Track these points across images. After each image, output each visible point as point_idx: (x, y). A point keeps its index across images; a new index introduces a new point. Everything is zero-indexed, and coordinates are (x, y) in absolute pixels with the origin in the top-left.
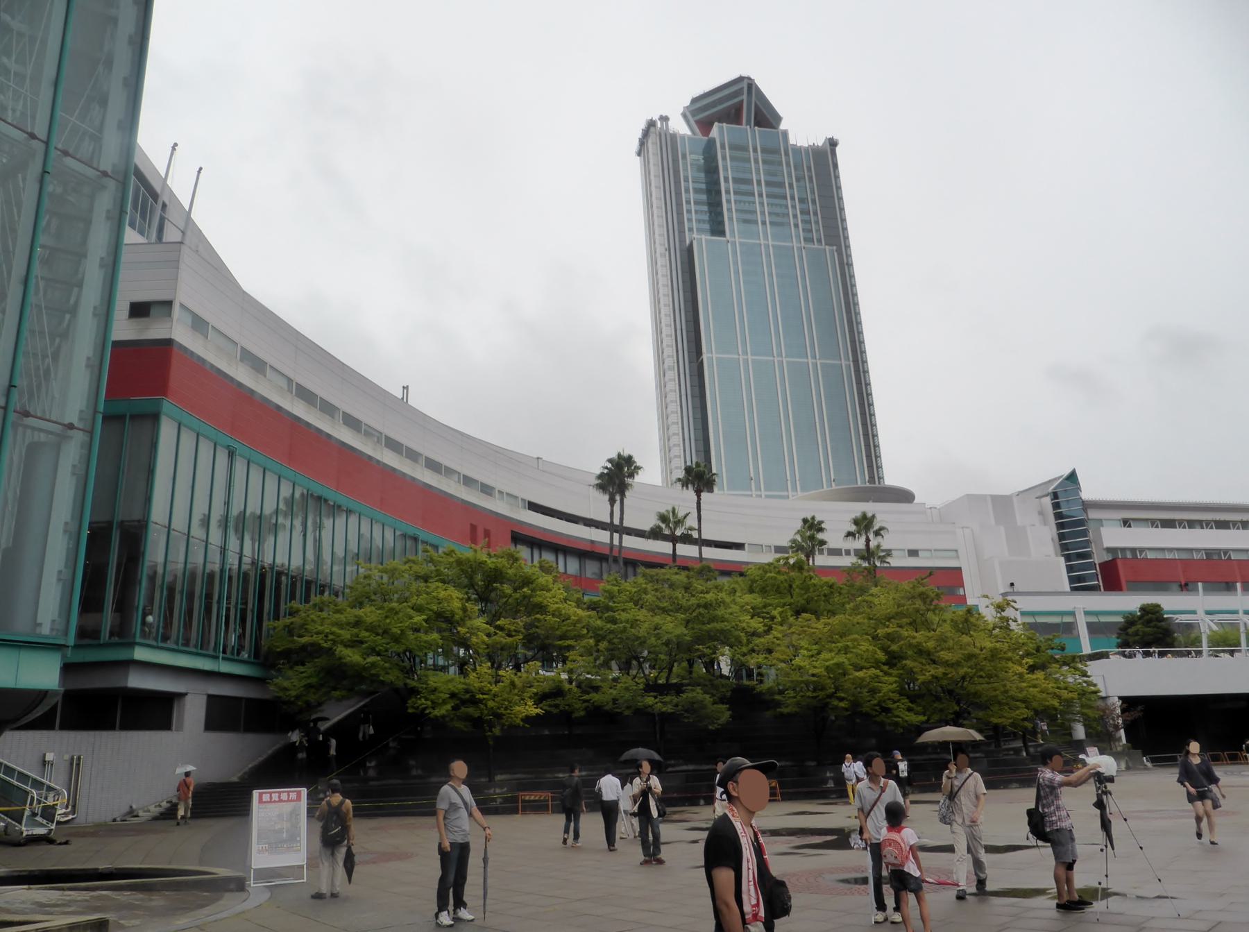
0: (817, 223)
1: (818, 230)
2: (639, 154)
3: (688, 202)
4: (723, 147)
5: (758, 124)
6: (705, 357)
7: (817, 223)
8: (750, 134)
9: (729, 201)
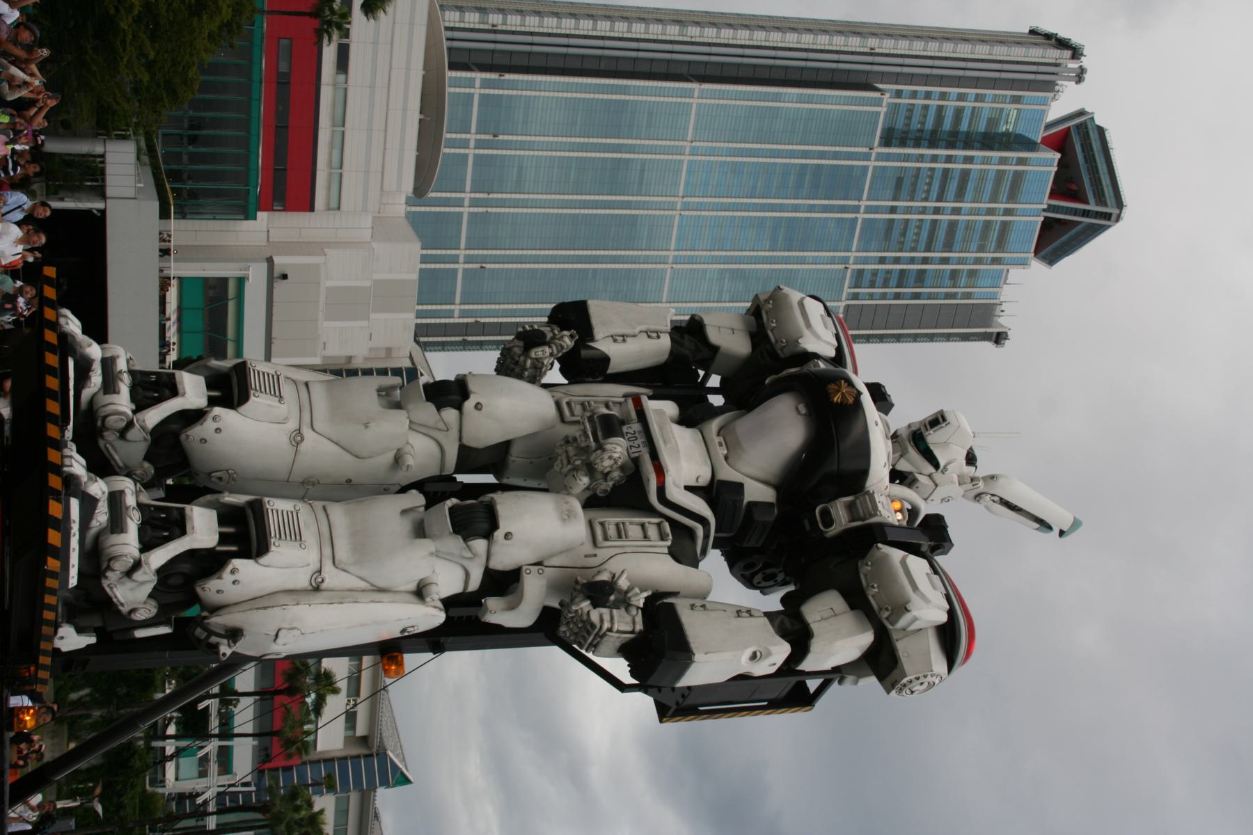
0: (884, 296)
1: (871, 297)
2: (1033, 32)
3: (943, 96)
4: (1021, 161)
5: (1048, 225)
6: (694, 86)
7: (884, 296)
8: (1031, 212)
9: (934, 159)
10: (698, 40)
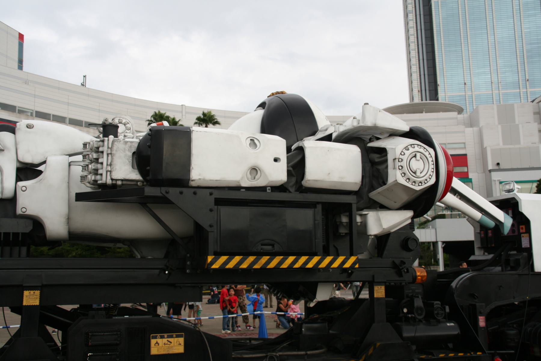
10: (413, 5)
